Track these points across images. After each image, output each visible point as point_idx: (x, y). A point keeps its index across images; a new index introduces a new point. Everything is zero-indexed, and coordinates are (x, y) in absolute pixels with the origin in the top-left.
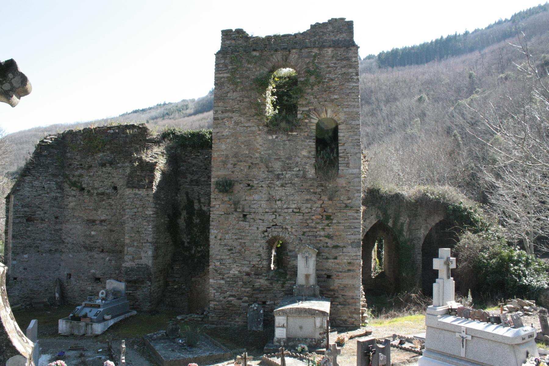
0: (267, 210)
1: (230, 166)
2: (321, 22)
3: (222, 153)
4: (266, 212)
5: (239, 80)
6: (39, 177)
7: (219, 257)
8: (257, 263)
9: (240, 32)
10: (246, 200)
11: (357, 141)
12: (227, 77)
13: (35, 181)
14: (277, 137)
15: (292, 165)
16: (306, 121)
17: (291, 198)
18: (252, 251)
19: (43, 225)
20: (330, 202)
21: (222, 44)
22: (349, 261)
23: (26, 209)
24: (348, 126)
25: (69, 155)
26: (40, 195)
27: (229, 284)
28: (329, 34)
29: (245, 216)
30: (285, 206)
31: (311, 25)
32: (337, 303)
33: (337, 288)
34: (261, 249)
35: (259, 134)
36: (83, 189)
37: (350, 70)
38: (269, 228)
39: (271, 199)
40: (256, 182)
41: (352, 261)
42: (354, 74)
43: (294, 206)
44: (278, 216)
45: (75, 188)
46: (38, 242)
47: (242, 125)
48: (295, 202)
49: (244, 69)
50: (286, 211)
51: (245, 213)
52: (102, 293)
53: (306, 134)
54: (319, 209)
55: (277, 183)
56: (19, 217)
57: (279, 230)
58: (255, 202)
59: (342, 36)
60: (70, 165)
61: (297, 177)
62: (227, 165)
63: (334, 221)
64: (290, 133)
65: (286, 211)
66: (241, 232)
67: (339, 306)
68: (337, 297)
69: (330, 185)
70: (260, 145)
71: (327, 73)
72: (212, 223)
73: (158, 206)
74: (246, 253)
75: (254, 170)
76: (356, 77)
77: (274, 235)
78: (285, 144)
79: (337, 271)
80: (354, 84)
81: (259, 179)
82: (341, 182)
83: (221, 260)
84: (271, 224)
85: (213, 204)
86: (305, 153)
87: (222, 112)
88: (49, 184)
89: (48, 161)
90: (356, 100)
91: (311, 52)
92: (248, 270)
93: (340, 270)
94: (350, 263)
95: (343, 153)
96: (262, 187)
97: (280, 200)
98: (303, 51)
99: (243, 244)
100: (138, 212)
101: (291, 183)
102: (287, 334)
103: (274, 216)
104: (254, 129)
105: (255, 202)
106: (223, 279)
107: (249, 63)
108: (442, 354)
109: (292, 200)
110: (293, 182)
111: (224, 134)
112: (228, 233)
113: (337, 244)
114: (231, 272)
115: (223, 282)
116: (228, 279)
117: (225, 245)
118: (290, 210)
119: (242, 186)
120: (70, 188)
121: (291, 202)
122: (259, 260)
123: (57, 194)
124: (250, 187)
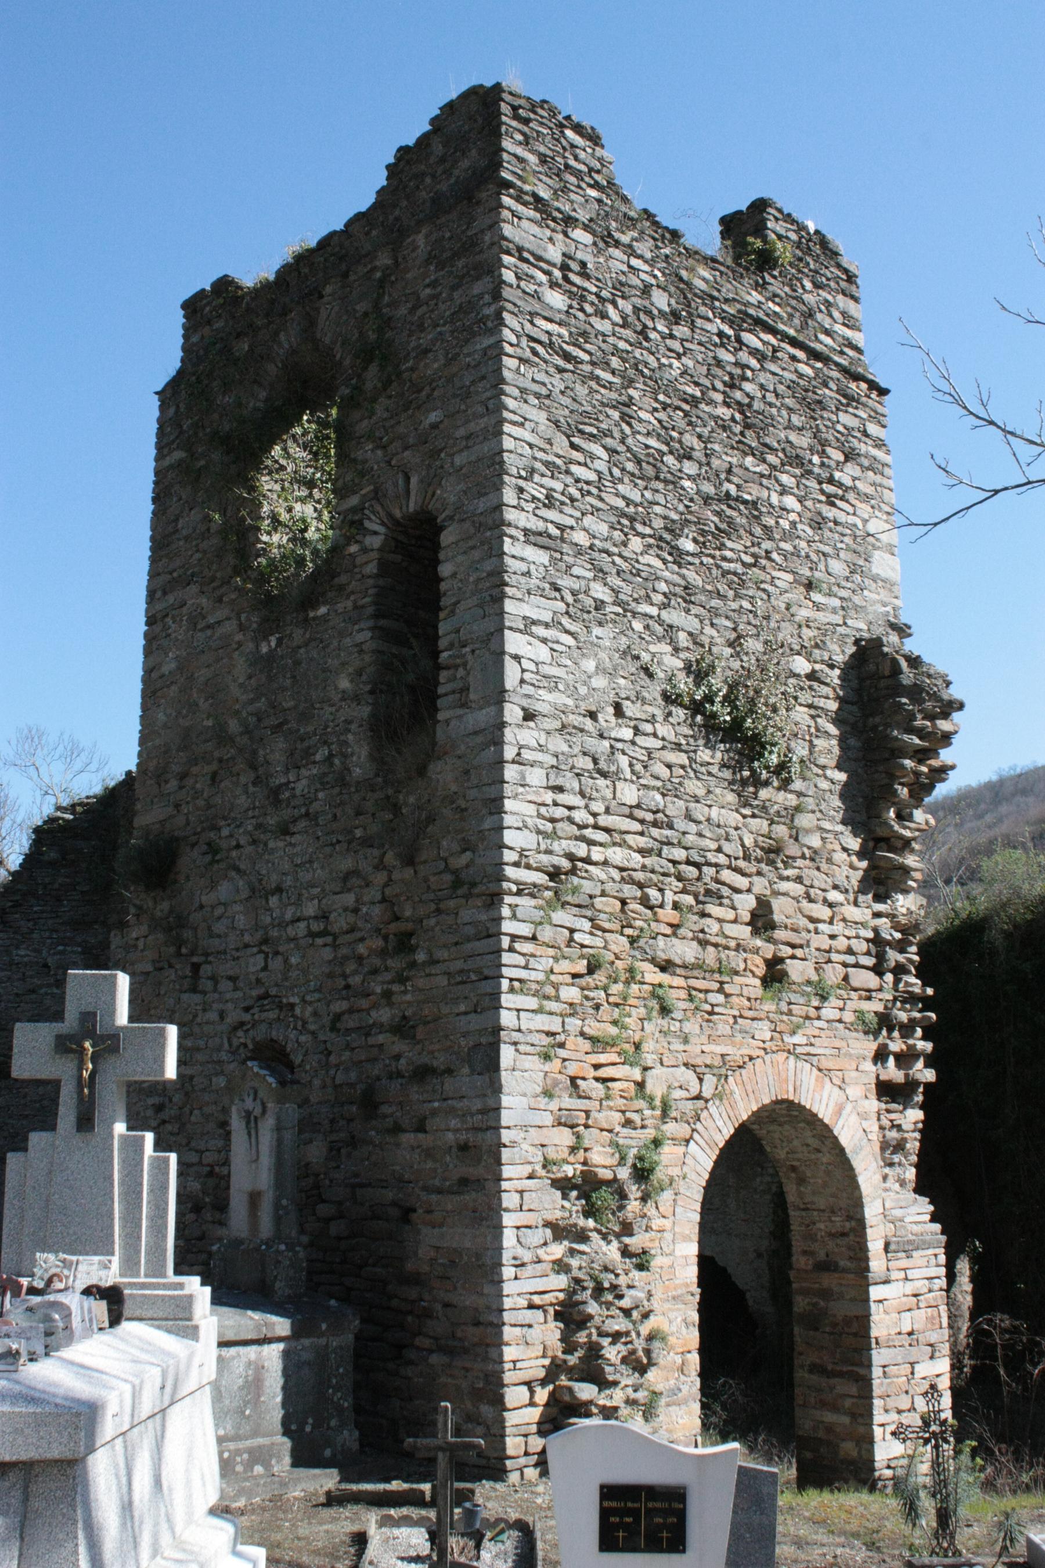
0: (247, 938)
2: (411, 142)
6: (32, 931)
9: (224, 285)
13: (17, 948)
14: (280, 642)
17: (305, 876)
20: (409, 872)
22: (463, 1137)
24: (467, 525)
26: (33, 991)
30: (288, 916)
32: (426, 1343)
33: (426, 1268)
35: (240, 644)
37: (478, 288)
40: (225, 832)
41: (470, 1136)
42: (487, 298)
43: (310, 909)
48: (316, 891)
51: (195, 959)
54: (377, 910)
57: (272, 1015)
62: (166, 782)
63: (421, 957)
64: (312, 614)
65: (291, 931)
67: (435, 1359)
68: (428, 1314)
69: (412, 800)
70: (241, 685)
78: (297, 663)
79: (425, 1188)
82: (444, 774)
84: (254, 993)
86: (344, 684)
87: (165, 593)
88: (61, 953)
89: (60, 880)
91: (374, 269)
93: (437, 1182)
94: (464, 1148)
95: (451, 646)
96: (238, 846)
101: (307, 814)
108: (135, 1542)
113: (425, 1059)
119: (195, 853)
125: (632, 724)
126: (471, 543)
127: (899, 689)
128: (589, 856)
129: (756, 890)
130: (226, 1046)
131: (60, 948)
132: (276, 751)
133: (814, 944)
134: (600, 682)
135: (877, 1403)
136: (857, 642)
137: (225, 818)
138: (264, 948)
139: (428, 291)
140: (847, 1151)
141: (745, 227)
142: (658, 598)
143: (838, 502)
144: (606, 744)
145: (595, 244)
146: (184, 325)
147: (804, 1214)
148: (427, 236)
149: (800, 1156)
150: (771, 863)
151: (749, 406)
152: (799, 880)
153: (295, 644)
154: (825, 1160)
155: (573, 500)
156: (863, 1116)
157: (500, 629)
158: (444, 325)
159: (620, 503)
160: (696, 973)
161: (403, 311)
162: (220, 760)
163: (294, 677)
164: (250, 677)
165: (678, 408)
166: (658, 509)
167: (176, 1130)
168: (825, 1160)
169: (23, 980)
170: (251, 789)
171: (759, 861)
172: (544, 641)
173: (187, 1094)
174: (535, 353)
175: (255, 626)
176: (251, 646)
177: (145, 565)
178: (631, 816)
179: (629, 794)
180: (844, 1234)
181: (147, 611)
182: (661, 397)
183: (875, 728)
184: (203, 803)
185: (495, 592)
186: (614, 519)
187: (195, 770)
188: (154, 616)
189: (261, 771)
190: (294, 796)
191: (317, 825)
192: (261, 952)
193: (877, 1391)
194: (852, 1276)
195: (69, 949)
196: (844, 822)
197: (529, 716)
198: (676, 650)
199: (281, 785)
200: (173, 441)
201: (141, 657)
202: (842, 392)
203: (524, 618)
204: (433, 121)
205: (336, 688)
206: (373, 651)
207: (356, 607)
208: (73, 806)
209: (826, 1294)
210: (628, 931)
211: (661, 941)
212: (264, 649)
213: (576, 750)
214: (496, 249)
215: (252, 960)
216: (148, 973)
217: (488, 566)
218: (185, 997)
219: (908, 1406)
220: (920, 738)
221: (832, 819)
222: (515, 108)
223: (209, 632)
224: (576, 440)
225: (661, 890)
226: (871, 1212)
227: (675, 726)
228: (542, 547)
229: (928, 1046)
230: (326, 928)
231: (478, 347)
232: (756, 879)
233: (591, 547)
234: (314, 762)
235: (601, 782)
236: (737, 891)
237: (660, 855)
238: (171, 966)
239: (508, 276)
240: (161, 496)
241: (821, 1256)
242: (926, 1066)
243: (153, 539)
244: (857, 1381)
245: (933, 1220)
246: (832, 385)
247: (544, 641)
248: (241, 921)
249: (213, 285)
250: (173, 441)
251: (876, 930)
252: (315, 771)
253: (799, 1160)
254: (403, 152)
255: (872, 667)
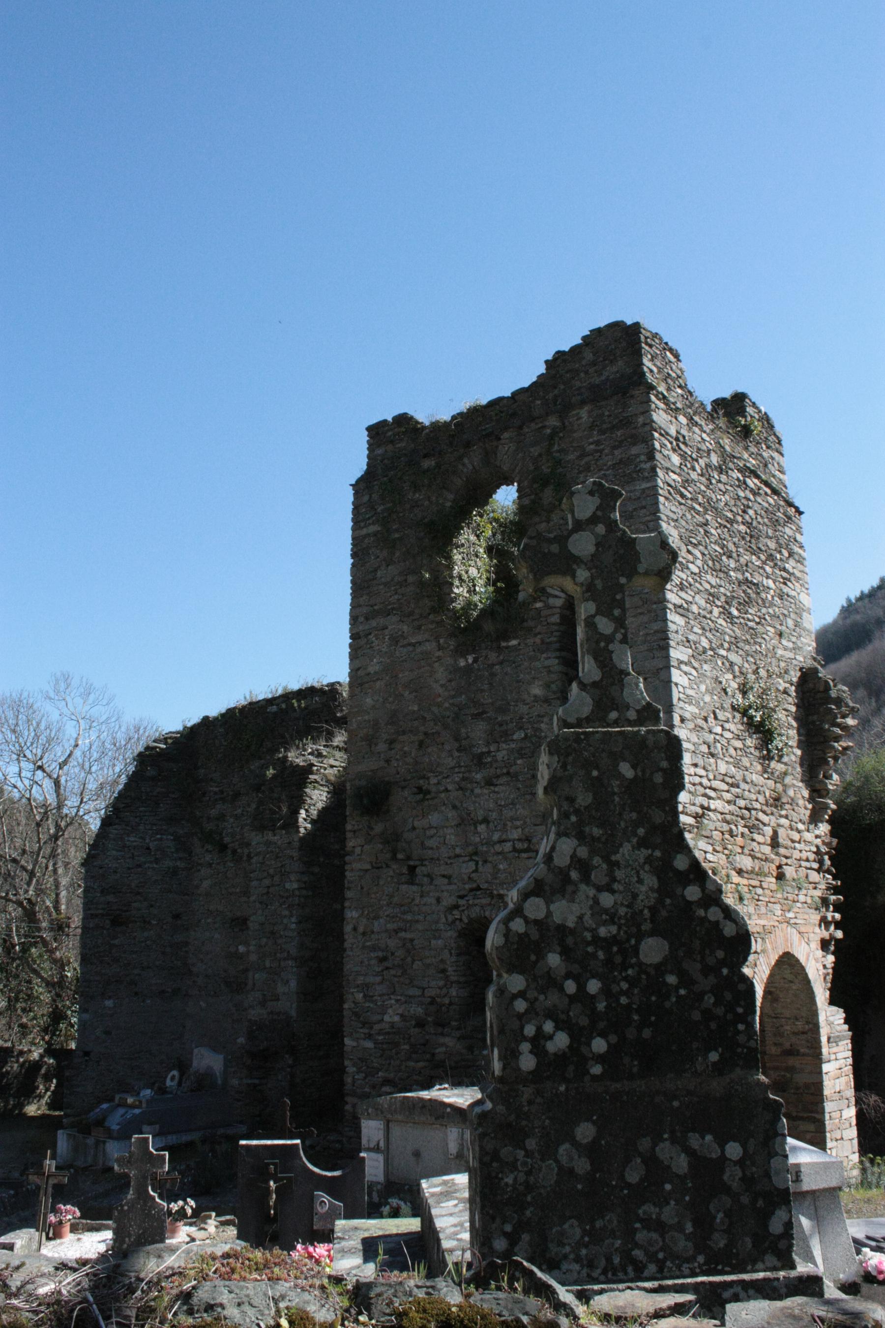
0: (458, 851)
1: (382, 747)
2: (566, 348)
3: (366, 718)
4: (458, 856)
5: (397, 536)
7: (360, 980)
8: (438, 991)
9: (403, 420)
10: (414, 828)
11: (659, 635)
12: (375, 534)
13: (128, 835)
14: (475, 660)
15: (511, 726)
16: (539, 605)
17: (508, 813)
18: (428, 961)
19: (146, 934)
21: (369, 457)
23: (111, 898)
25: (202, 771)
26: (139, 866)
27: (383, 1050)
28: (586, 373)
29: (412, 869)
30: (496, 837)
31: (547, 362)
34: (446, 955)
35: (439, 659)
36: (223, 848)
37: (634, 450)
38: (461, 897)
39: (466, 822)
40: (434, 781)
42: (643, 458)
43: (515, 834)
44: (480, 863)
45: (210, 847)
46: (136, 972)
47: (405, 642)
48: (518, 823)
49: (408, 506)
50: (498, 848)
51: (412, 863)
52: (173, 1078)
53: (538, 640)
55: (479, 776)
56: (97, 916)
57: (484, 901)
58: (433, 831)
59: (614, 369)
60: (204, 794)
61: (522, 756)
62: (376, 745)
64: (504, 644)
65: (498, 848)
66: (404, 913)
70: (442, 686)
71: (580, 472)
72: (349, 894)
73: (316, 870)
74: (415, 966)
75: (429, 750)
76: (648, 466)
77: (473, 915)
78: (493, 675)
80: (645, 485)
81: (441, 773)
83: (366, 986)
84: (467, 887)
85: (350, 844)
86: (537, 690)
87: (367, 619)
88: (161, 839)
90: (651, 525)
91: (544, 427)
92: (420, 1011)
96: (447, 790)
97: (486, 821)
98: (526, 430)
99: (409, 945)
100: (273, 885)
101: (508, 773)
102: (387, 1173)
103: (472, 865)
104: (428, 647)
105: (433, 831)
106: (369, 1037)
107: (416, 488)
109: (512, 819)
110: (513, 770)
111: (371, 670)
112: (377, 918)
114: (387, 1018)
115: (369, 1044)
116: (381, 1038)
117: (374, 948)
118: (508, 846)
119: (406, 793)
120: (203, 847)
121: (509, 824)
122: (441, 983)
123: (178, 863)
124: (421, 796)
125: (720, 723)
126: (639, 611)
127: (829, 700)
128: (709, 806)
129: (772, 824)
130: (444, 920)
131: (159, 836)
132: (478, 731)
133: (794, 856)
134: (707, 698)
135: (828, 1135)
136: (801, 669)
137: (431, 771)
138: (474, 858)
139: (592, 447)
140: (812, 982)
141: (733, 408)
142: (726, 645)
143: (788, 583)
144: (712, 736)
145: (688, 424)
146: (368, 441)
147: (774, 1020)
148: (589, 412)
149: (777, 985)
150: (776, 807)
151: (751, 524)
152: (786, 817)
153: (490, 662)
154: (794, 987)
155: (691, 585)
156: (816, 960)
157: (668, 667)
158: (607, 470)
159: (708, 587)
160: (751, 876)
161: (571, 457)
162: (426, 734)
163: (491, 684)
164: (450, 681)
165: (725, 527)
166: (722, 590)
167: (399, 974)
168: (794, 987)
169: (133, 858)
170: (456, 754)
171: (771, 806)
172: (686, 673)
173: (408, 951)
174: (670, 493)
175: (452, 647)
176: (449, 661)
177: (348, 599)
178: (723, 781)
179: (723, 767)
180: (803, 1033)
181: (351, 630)
182: (719, 520)
183: (813, 722)
184: (412, 761)
185: (662, 643)
186: (706, 597)
187: (401, 738)
188: (358, 633)
189: (464, 742)
190: (496, 761)
191: (518, 780)
192: (471, 860)
193: (828, 1128)
194: (810, 1058)
195: (165, 837)
196: (802, 781)
197: (683, 720)
198: (734, 677)
199: (483, 753)
200: (369, 518)
201: (347, 661)
202: (785, 514)
203: (678, 659)
204: (584, 338)
205: (529, 694)
206: (560, 672)
207: (543, 642)
208: (166, 739)
209: (791, 1069)
210: (726, 852)
211: (738, 857)
212: (462, 663)
213: (701, 741)
214: (647, 428)
215: (464, 865)
216: (367, 871)
217: (656, 626)
218: (404, 887)
219: (839, 1137)
220: (841, 729)
221: (796, 779)
222: (646, 338)
223: (411, 648)
224: (689, 547)
225: (736, 826)
226: (822, 1018)
227: (735, 726)
228: (682, 615)
229: (838, 916)
230: (529, 847)
231: (638, 488)
232: (771, 817)
233: (699, 614)
234: (512, 740)
235: (712, 760)
236: (765, 825)
237: (735, 804)
238: (387, 866)
239: (657, 445)
240: (359, 552)
241: (787, 1045)
242: (836, 928)
243: (352, 582)
244: (814, 1122)
245: (845, 1023)
246: (781, 510)
247: (686, 673)
248: (451, 839)
249: (394, 418)
250: (369, 518)
251: (817, 847)
252: (514, 746)
253: (775, 987)
254: (559, 355)
255: (811, 685)
